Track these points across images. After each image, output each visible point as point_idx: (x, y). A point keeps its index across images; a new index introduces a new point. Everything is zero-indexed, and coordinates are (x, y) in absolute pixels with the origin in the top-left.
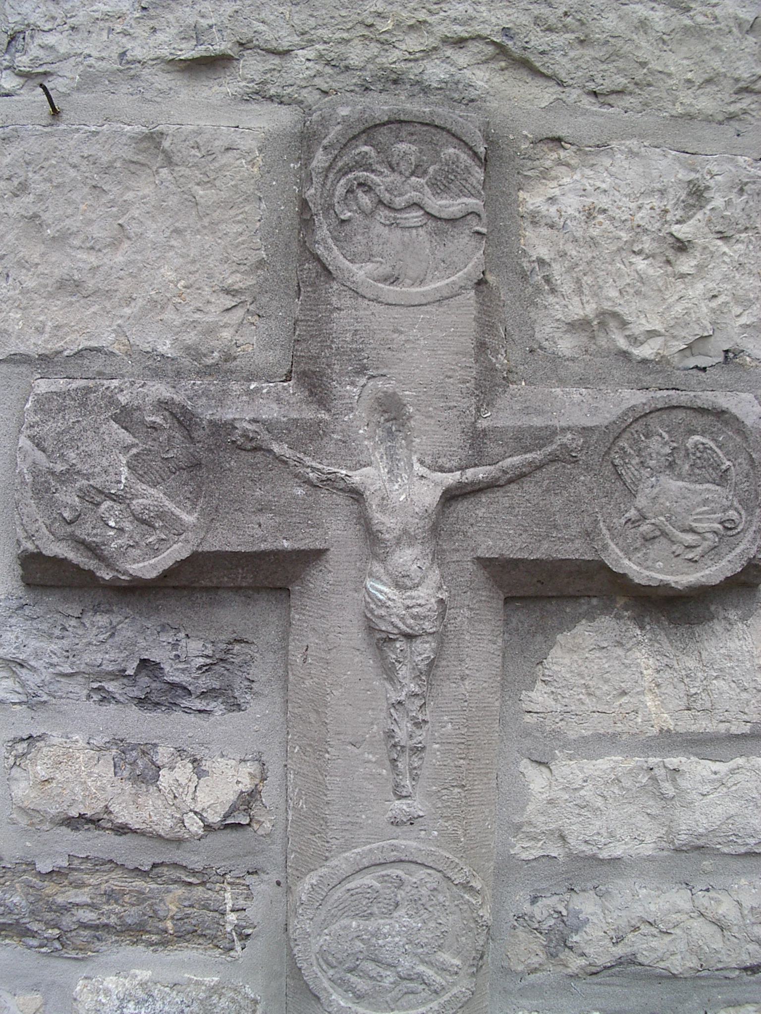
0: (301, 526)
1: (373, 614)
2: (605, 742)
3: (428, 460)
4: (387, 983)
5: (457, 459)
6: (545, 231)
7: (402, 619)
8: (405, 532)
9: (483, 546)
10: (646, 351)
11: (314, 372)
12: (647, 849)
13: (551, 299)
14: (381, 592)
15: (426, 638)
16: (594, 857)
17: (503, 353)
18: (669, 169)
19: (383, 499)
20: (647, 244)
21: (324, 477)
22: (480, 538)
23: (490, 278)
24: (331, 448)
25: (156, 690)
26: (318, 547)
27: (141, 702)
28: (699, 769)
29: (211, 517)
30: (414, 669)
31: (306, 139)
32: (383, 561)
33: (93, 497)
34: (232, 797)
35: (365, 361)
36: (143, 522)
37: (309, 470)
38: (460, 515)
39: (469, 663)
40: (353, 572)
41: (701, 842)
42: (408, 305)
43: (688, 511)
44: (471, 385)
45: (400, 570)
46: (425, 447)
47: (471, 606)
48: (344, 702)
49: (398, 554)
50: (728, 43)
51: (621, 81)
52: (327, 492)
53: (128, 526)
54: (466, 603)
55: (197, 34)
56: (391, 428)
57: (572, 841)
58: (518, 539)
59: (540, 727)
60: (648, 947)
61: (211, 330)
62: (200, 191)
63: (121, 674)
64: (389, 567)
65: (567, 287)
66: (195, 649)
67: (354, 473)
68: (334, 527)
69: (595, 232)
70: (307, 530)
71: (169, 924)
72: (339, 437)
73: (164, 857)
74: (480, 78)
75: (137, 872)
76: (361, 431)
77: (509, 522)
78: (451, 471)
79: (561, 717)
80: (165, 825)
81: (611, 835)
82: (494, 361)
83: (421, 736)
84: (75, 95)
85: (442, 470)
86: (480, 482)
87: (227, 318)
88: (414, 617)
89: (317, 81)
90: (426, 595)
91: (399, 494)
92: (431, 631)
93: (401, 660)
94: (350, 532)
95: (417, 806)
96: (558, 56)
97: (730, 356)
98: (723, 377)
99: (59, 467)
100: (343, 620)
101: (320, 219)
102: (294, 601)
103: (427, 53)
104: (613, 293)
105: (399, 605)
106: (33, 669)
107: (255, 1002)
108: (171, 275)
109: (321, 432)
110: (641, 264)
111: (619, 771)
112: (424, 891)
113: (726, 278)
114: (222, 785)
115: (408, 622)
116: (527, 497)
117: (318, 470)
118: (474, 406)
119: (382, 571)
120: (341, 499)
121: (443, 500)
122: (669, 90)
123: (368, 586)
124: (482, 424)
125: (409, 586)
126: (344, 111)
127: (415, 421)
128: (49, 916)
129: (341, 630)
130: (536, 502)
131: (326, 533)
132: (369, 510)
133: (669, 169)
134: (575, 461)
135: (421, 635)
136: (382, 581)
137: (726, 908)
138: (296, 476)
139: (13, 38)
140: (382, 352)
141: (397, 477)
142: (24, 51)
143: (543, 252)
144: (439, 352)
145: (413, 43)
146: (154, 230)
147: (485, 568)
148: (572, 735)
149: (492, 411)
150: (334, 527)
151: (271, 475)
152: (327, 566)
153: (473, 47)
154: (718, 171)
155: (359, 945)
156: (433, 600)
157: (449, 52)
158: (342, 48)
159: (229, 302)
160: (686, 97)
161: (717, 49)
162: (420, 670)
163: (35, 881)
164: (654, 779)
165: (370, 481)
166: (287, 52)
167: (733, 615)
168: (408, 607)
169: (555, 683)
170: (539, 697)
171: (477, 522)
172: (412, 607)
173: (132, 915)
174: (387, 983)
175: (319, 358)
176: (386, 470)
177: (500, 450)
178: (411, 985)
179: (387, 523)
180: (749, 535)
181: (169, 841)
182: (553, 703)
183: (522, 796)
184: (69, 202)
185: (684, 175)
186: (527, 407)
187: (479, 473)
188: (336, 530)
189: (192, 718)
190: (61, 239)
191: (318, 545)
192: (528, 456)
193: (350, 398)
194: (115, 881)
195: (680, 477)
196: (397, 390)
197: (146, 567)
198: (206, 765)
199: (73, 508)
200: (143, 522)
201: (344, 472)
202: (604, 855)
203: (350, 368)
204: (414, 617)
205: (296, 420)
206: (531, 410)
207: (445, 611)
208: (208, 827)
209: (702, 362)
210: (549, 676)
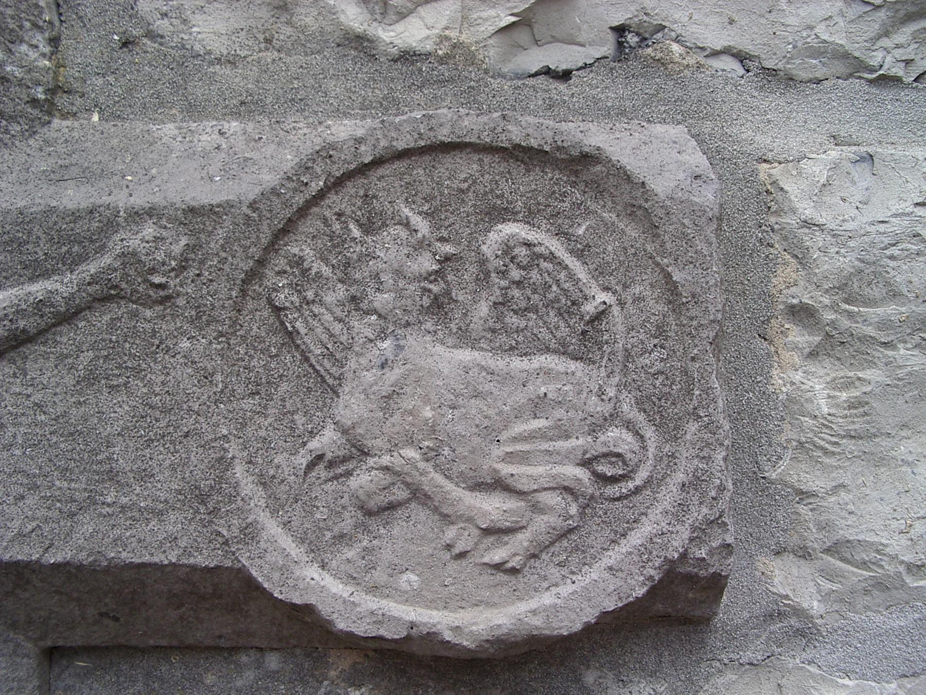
43: (491, 433)
98: (613, 90)
116: (37, 397)
180: (669, 495)
195: (465, 338)
209: (559, 57)
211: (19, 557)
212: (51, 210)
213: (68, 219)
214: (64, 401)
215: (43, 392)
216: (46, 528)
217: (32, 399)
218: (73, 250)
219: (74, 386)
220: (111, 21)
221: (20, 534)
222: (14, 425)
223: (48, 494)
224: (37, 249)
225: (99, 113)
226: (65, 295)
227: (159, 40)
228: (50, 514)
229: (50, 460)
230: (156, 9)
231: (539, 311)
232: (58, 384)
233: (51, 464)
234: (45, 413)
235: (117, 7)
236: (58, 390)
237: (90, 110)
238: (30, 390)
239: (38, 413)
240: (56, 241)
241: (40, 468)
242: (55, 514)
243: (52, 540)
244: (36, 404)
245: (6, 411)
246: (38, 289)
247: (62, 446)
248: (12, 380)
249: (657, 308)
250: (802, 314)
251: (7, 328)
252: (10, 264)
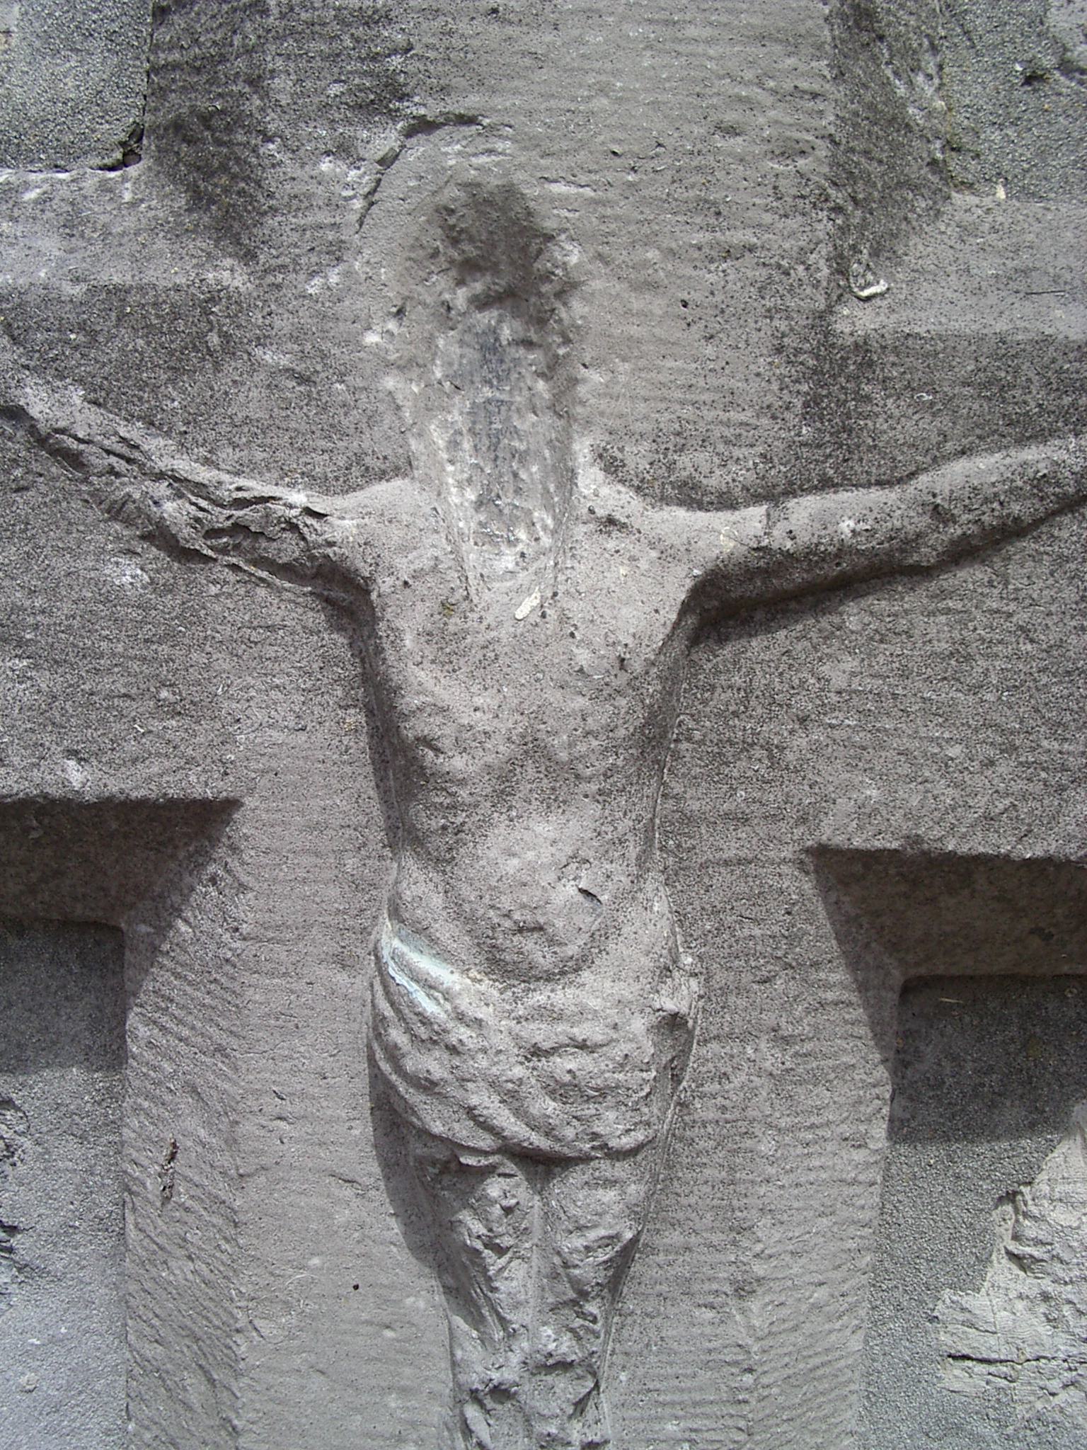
0: (132, 708)
1: (399, 1070)
3: (637, 457)
5: (750, 455)
7: (512, 1097)
8: (532, 748)
9: (845, 806)
11: (206, 120)
14: (430, 986)
15: (606, 1168)
17: (932, 69)
19: (447, 608)
21: (220, 517)
22: (833, 774)
24: (252, 401)
26: (198, 792)
30: (554, 1276)
32: (442, 862)
35: (396, 61)
37: (162, 489)
38: (760, 681)
39: (768, 1234)
40: (333, 892)
44: (815, 164)
45: (506, 903)
46: (623, 406)
47: (787, 1030)
48: (297, 1361)
49: (499, 835)
52: (232, 577)
54: (769, 1019)
56: (494, 331)
58: (979, 781)
64: (467, 892)
67: (340, 502)
68: (260, 716)
70: (156, 725)
72: (285, 361)
76: (371, 338)
77: (945, 714)
78: (726, 502)
79: (1068, 1376)
82: (902, 91)
85: (691, 495)
86: (843, 550)
88: (561, 1090)
90: (609, 1005)
91: (510, 586)
92: (627, 1142)
93: (506, 1241)
94: (319, 737)
100: (294, 1071)
105: (500, 1041)
109: (214, 339)
115: (534, 1110)
116: (1022, 617)
117: (200, 489)
118: (824, 250)
119: (437, 900)
120: (290, 609)
121: (691, 621)
123: (386, 954)
124: (855, 321)
125: (562, 956)
127: (586, 300)
129: (288, 1108)
130: (1053, 637)
131: (227, 740)
132: (390, 655)
135: (585, 1159)
136: (433, 941)
138: (117, 511)
140: (463, 26)
141: (510, 524)
144: (691, 31)
147: (845, 882)
149: (890, 277)
150: (260, 716)
151: (23, 510)
152: (234, 863)
156: (638, 1025)
162: (575, 1283)
165: (396, 535)
168: (537, 1052)
169: (1057, 1268)
170: (1000, 1306)
171: (825, 709)
172: (553, 1051)
175: (223, 59)
176: (471, 495)
177: (926, 427)
179: (451, 703)
182: (1044, 1330)
186: (1025, 272)
187: (838, 516)
188: (269, 732)
191: (199, 785)
192: (1032, 454)
193: (333, 204)
196: (519, 176)
201: (299, 498)
203: (335, 89)
204: (561, 1090)
205: (119, 292)
206: (1039, 281)
207: (685, 1052)
210: (1038, 1242)
211: (981, 849)
212: (1047, 340)
213: (1071, 356)
214: (1061, 625)
215: (1031, 609)
216: (1024, 809)
217: (1014, 620)
218: (1080, 402)
219: (1077, 603)
220: (1012, 41)
221: (989, 818)
222: (987, 657)
223: (1031, 759)
224: (1028, 398)
225: (1005, 186)
226: (1076, 469)
227: (1077, 75)
228: (1031, 787)
229: (1037, 711)
230: (1079, 26)
232: (1054, 600)
233: (1037, 716)
234: (1032, 641)
235: (1022, 19)
236: (1053, 609)
237: (990, 180)
238: (1012, 607)
239: (1021, 640)
240: (1055, 386)
241: (1021, 722)
242: (1037, 788)
243: (1029, 825)
244: (1021, 628)
245: (974, 636)
246: (1036, 456)
247: (1055, 689)
248: (986, 591)
251: (996, 513)
252: (988, 417)
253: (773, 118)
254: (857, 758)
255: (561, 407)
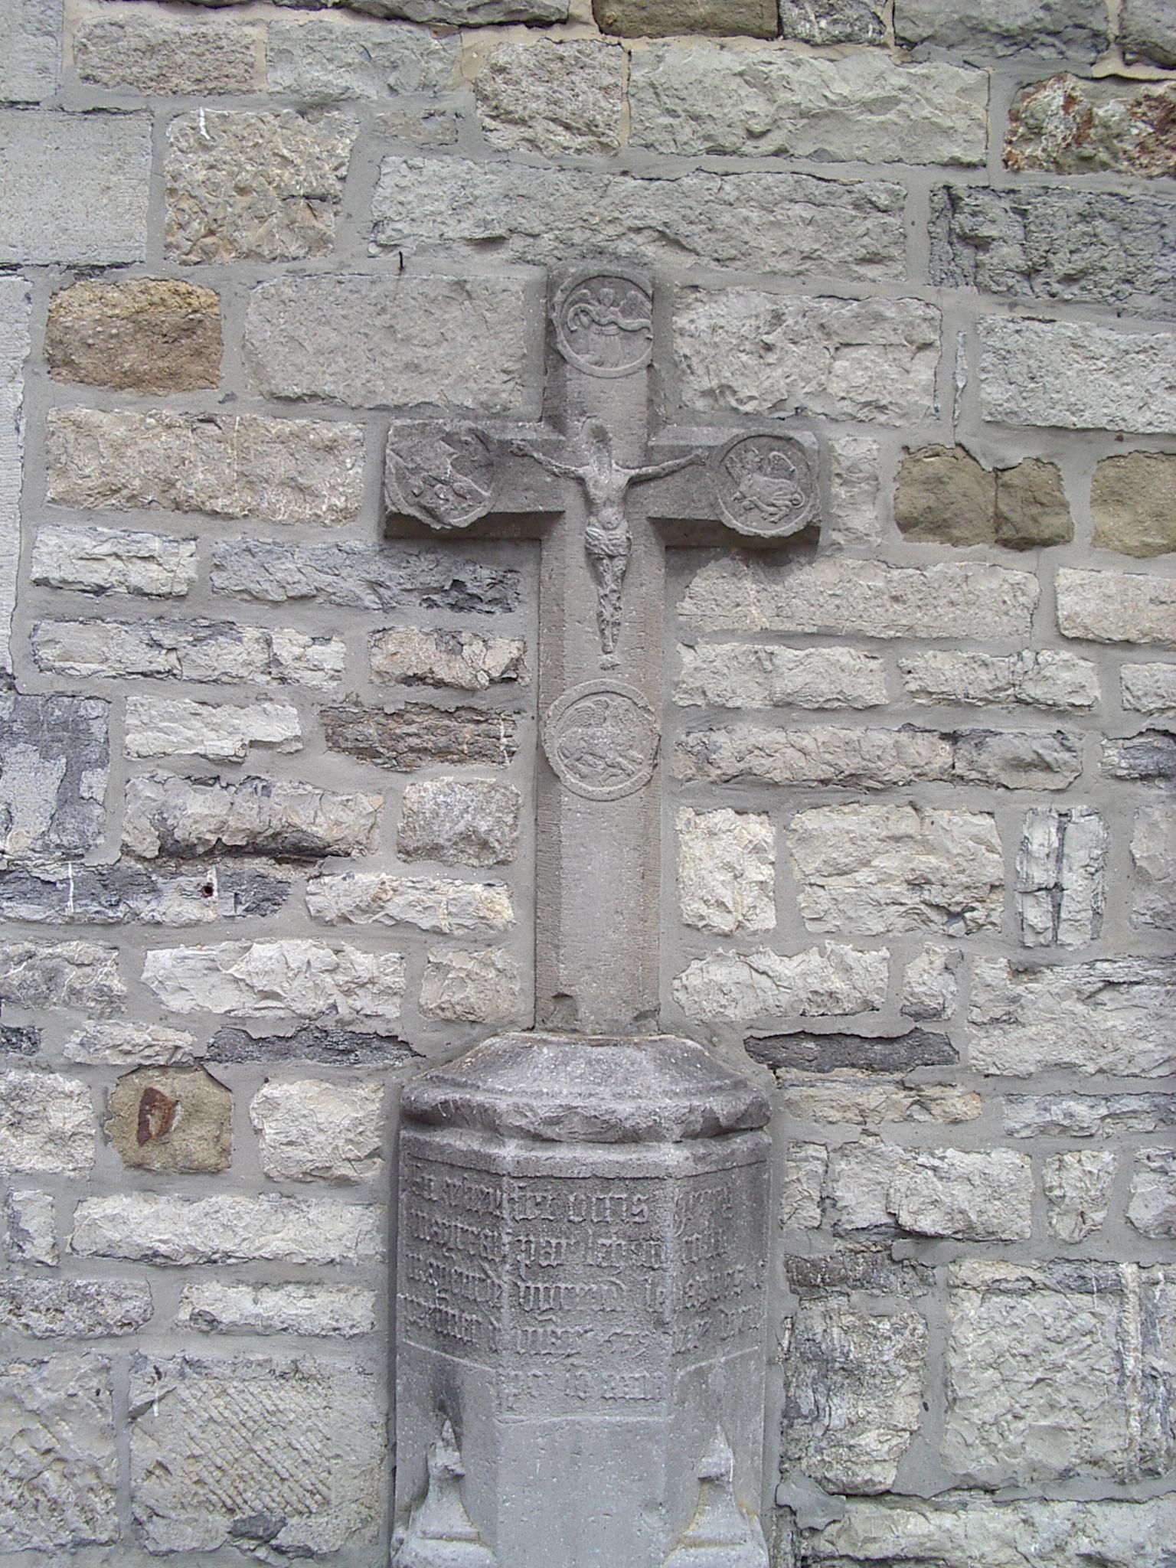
2: (729, 634)
4: (599, 769)
6: (688, 339)
10: (748, 408)
12: (757, 705)
13: (692, 378)
16: (723, 706)
18: (761, 303)
20: (748, 346)
23: (656, 365)
24: (566, 455)
25: (463, 599)
27: (452, 606)
28: (786, 655)
29: (499, 493)
31: (550, 286)
33: (433, 481)
34: (507, 661)
36: (460, 495)
41: (790, 699)
42: (608, 377)
43: (771, 494)
50: (796, 231)
51: (734, 252)
53: (451, 498)
55: (485, 224)
57: (709, 694)
59: (688, 624)
60: (758, 763)
61: (495, 393)
62: (488, 315)
63: (441, 590)
65: (701, 371)
66: (485, 573)
69: (717, 339)
71: (465, 747)
73: (465, 704)
74: (651, 251)
75: (449, 714)
80: (466, 679)
81: (734, 692)
83: (618, 616)
84: (414, 258)
87: (504, 386)
89: (555, 252)
90: (620, 534)
91: (604, 480)
95: (615, 658)
96: (696, 238)
97: (799, 411)
98: (795, 423)
99: (411, 466)
101: (559, 330)
102: (545, 545)
103: (619, 236)
104: (728, 374)
106: (388, 587)
107: (517, 795)
108: (472, 362)
110: (744, 357)
111: (737, 652)
112: (621, 711)
113: (795, 365)
114: (496, 660)
120: (572, 484)
122: (762, 258)
124: (650, 444)
125: (612, 529)
126: (572, 270)
128: (390, 743)
133: (761, 303)
134: (704, 464)
137: (807, 742)
139: (376, 225)
142: (383, 232)
143: (687, 351)
145: (611, 230)
146: (462, 337)
148: (708, 630)
153: (646, 233)
154: (790, 304)
155: (583, 744)
157: (632, 235)
158: (569, 233)
159: (506, 378)
160: (772, 261)
161: (790, 234)
163: (383, 721)
164: (758, 659)
166: (537, 236)
167: (803, 560)
170: (687, 605)
173: (443, 741)
174: (599, 769)
178: (614, 770)
180: (808, 508)
181: (467, 690)
183: (679, 665)
184: (411, 319)
185: (769, 306)
187: (650, 470)
188: (569, 500)
189: (483, 616)
190: (407, 340)
191: (560, 509)
194: (431, 720)
195: (766, 475)
197: (462, 521)
198: (491, 643)
199: (419, 488)
200: (460, 495)
202: (730, 705)
208: (491, 680)
209: (782, 414)
231: (779, 470)
249: (805, 470)
250: (838, 475)
253: (638, 416)
254: (654, 504)
255: (610, 456)
